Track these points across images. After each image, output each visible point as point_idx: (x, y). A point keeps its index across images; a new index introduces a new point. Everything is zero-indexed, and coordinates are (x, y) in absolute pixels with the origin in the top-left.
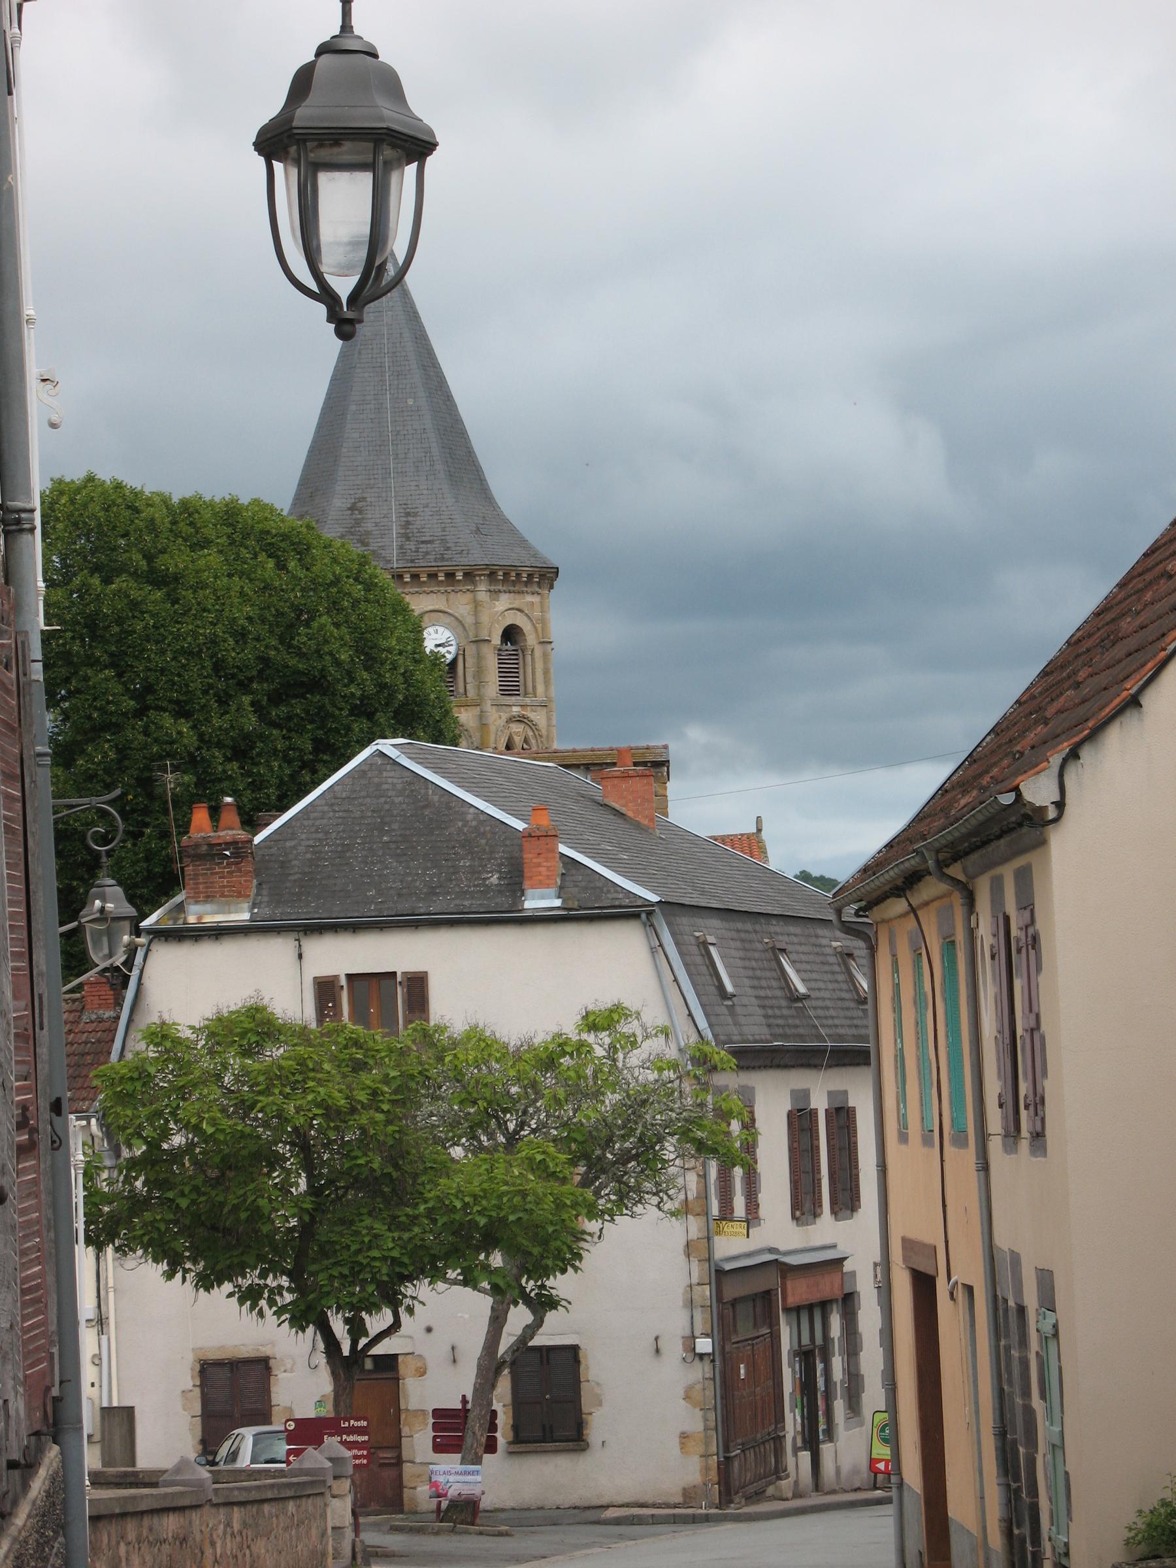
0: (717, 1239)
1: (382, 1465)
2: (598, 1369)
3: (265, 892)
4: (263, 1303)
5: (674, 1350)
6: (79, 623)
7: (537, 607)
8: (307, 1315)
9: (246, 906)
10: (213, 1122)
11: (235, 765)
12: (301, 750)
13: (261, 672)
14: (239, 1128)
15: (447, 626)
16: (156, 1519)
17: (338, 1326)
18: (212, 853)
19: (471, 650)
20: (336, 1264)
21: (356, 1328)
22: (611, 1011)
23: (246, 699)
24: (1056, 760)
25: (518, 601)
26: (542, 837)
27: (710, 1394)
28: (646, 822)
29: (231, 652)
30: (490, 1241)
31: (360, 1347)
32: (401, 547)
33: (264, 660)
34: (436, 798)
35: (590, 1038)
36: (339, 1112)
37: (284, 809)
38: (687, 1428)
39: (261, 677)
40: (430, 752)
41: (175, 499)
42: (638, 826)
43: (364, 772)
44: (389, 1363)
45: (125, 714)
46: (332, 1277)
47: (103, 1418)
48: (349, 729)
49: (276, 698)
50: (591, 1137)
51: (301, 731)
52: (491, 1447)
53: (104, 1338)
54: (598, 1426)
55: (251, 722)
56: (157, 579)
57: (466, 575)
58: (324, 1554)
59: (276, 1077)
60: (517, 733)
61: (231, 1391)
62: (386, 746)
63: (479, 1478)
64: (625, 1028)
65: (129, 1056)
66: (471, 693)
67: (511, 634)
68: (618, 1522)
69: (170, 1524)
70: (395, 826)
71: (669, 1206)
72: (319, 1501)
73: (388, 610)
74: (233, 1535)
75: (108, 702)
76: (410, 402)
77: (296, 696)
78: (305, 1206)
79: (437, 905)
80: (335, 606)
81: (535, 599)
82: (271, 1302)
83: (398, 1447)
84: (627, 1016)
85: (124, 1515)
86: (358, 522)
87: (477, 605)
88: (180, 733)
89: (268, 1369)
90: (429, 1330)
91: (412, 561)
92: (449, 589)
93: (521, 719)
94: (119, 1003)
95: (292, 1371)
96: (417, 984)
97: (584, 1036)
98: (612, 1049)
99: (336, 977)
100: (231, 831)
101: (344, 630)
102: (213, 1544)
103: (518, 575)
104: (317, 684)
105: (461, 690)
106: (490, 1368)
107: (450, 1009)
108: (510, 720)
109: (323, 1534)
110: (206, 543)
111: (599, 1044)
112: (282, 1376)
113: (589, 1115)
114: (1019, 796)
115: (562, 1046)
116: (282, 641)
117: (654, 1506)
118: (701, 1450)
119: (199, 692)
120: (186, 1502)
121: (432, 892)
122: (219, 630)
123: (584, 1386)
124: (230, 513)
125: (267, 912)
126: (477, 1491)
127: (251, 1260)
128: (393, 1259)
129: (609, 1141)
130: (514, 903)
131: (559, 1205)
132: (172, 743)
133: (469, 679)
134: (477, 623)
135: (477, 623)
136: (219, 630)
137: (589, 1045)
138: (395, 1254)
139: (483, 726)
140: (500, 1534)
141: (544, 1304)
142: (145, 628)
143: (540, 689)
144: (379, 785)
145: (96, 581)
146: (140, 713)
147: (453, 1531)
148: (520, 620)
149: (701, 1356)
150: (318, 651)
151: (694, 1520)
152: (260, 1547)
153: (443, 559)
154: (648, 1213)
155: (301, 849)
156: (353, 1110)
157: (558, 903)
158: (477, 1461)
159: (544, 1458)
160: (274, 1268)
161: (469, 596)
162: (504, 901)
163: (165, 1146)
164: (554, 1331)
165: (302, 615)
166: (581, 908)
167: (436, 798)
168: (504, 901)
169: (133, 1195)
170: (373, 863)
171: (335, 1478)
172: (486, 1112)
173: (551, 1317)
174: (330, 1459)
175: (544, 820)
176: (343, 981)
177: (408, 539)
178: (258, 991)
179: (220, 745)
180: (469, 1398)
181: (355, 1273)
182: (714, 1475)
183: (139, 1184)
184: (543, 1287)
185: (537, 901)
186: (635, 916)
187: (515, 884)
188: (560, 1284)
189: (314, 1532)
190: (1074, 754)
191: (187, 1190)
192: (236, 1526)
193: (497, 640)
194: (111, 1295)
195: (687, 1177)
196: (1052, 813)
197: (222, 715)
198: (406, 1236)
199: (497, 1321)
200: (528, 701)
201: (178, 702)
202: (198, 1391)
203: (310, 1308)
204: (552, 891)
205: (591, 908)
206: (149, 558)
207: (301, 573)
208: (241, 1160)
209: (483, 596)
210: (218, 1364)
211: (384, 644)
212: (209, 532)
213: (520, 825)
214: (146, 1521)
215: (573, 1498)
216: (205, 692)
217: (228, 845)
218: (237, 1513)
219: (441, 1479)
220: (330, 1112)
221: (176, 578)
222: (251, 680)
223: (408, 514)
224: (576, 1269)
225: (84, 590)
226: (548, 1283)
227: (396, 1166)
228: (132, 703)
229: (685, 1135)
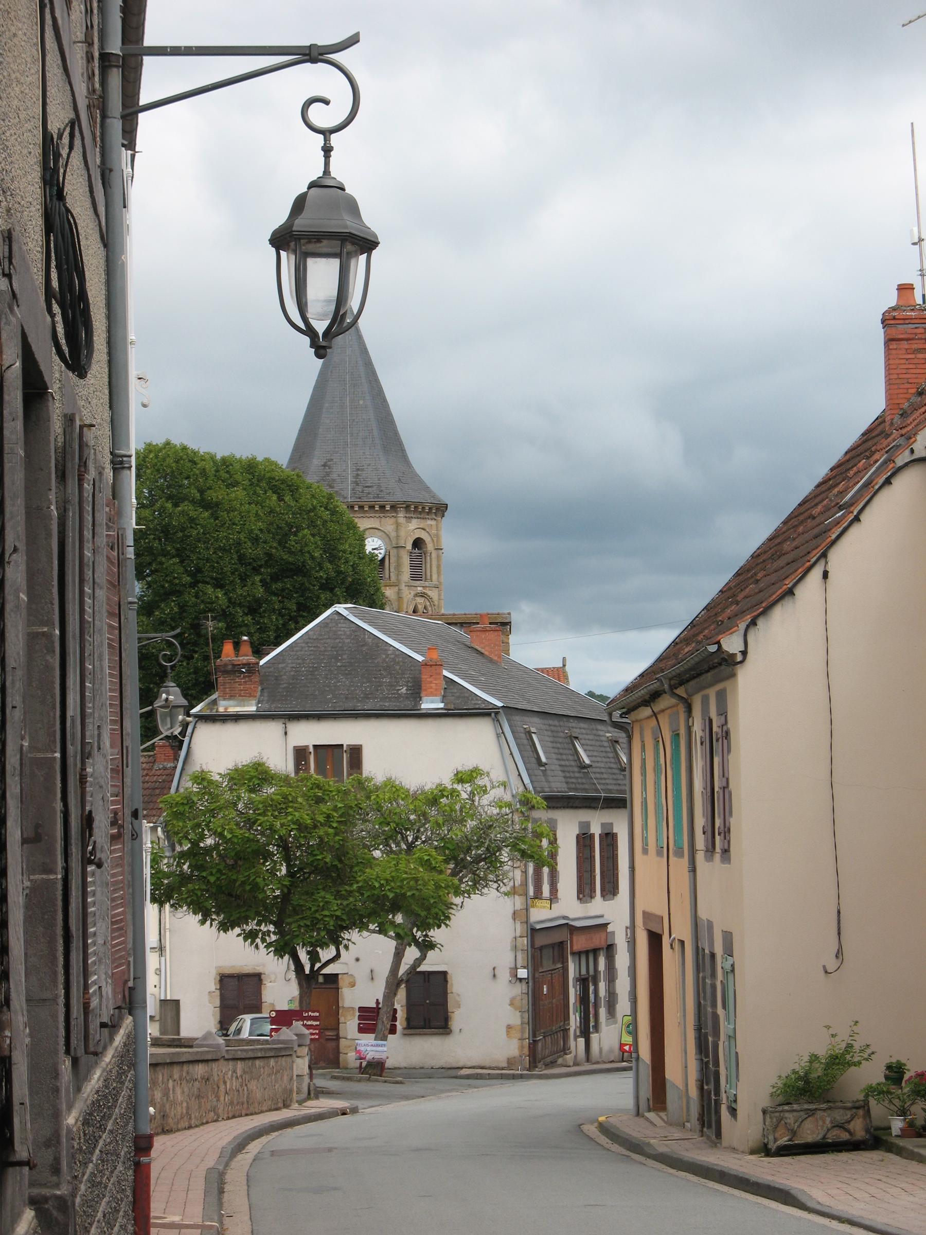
0: (532, 910)
1: (327, 1040)
2: (458, 986)
3: (266, 694)
4: (258, 940)
5: (504, 975)
6: (157, 530)
7: (434, 528)
8: (283, 948)
9: (254, 702)
10: (231, 831)
11: (250, 618)
13: (266, 562)
16: (191, 1067)
18: (234, 670)
19: (393, 552)
20: (302, 918)
21: (314, 957)
22: (472, 771)
23: (257, 578)
24: (742, 626)
26: (433, 666)
27: (525, 1003)
28: (496, 658)
29: (249, 550)
30: (395, 907)
31: (316, 968)
32: (353, 489)
33: (269, 555)
34: (370, 640)
35: (459, 787)
36: (306, 827)
37: (278, 644)
38: (511, 1022)
39: (267, 564)
40: (368, 613)
41: (218, 457)
42: (491, 661)
43: (327, 624)
44: (333, 979)
45: (184, 585)
46: (300, 926)
47: (161, 1006)
48: (318, 597)
49: (275, 578)
51: (290, 598)
52: (393, 1030)
53: (163, 959)
54: (458, 1019)
56: (206, 505)
57: (392, 507)
58: (291, 1091)
59: (270, 806)
60: (420, 603)
61: (238, 992)
62: (341, 608)
63: (385, 1049)
64: (480, 782)
65: (182, 790)
66: (393, 578)
67: (418, 543)
68: (468, 1077)
69: (200, 1070)
70: (345, 657)
71: (503, 889)
72: (288, 1059)
73: (345, 528)
74: (237, 1077)
75: (175, 578)
76: (361, 402)
80: (312, 524)
81: (433, 523)
82: (263, 940)
83: (338, 1029)
84: (481, 775)
85: (172, 1064)
86: (328, 474)
87: (398, 525)
88: (217, 597)
89: (260, 980)
90: (357, 960)
93: (423, 595)
94: (176, 759)
95: (275, 982)
96: (356, 752)
97: (455, 786)
98: (472, 794)
99: (307, 746)
100: (246, 657)
101: (318, 538)
102: (225, 1083)
103: (423, 508)
104: (299, 570)
105: (387, 576)
106: (393, 983)
107: (375, 768)
109: (291, 1079)
110: (235, 484)
111: (464, 791)
112: (269, 984)
114: (720, 647)
116: (280, 543)
117: (490, 1068)
119: (229, 573)
120: (209, 1057)
121: (367, 697)
122: (242, 536)
123: (449, 996)
124: (251, 466)
125: (267, 706)
126: (384, 1056)
127: (252, 915)
128: (337, 917)
129: (469, 849)
130: (415, 705)
131: (438, 887)
134: (398, 536)
135: (398, 536)
136: (242, 536)
137: (458, 792)
138: (338, 913)
139: (400, 598)
140: (397, 1082)
141: (427, 946)
142: (198, 534)
143: (435, 577)
145: (169, 505)
146: (193, 585)
147: (369, 1080)
148: (423, 535)
149: (521, 980)
150: (301, 551)
151: (514, 1077)
152: (253, 1085)
153: (378, 497)
155: (288, 669)
156: (315, 827)
157: (442, 705)
158: (384, 1038)
159: (425, 1038)
160: (265, 920)
161: (393, 520)
162: (409, 704)
163: (202, 845)
165: (292, 529)
167: (370, 640)
170: (331, 679)
171: (299, 1046)
172: (394, 830)
173: (431, 954)
175: (435, 655)
176: (311, 749)
179: (240, 605)
180: (381, 1001)
181: (314, 924)
182: (526, 1051)
183: (185, 867)
184: (426, 936)
185: (430, 704)
186: (489, 715)
187: (416, 693)
188: (436, 934)
189: (285, 1077)
190: (753, 623)
191: (214, 871)
192: (239, 1073)
194: (168, 933)
195: (515, 872)
196: (739, 658)
198: (345, 903)
199: (399, 955)
200: (427, 584)
201: (216, 579)
202: (218, 993)
203: (286, 944)
204: (438, 698)
205: (462, 709)
206: (202, 492)
207: (293, 504)
208: (246, 855)
209: (402, 520)
210: (231, 976)
212: (238, 477)
213: (420, 658)
214: (185, 1067)
215: (442, 1062)
216: (233, 573)
217: (244, 665)
218: (240, 1065)
219: (362, 1049)
221: (217, 505)
222: (261, 566)
223: (358, 470)
224: (447, 925)
225: (162, 510)
226: (430, 934)
227: (341, 861)
228: (188, 578)
229: (514, 846)
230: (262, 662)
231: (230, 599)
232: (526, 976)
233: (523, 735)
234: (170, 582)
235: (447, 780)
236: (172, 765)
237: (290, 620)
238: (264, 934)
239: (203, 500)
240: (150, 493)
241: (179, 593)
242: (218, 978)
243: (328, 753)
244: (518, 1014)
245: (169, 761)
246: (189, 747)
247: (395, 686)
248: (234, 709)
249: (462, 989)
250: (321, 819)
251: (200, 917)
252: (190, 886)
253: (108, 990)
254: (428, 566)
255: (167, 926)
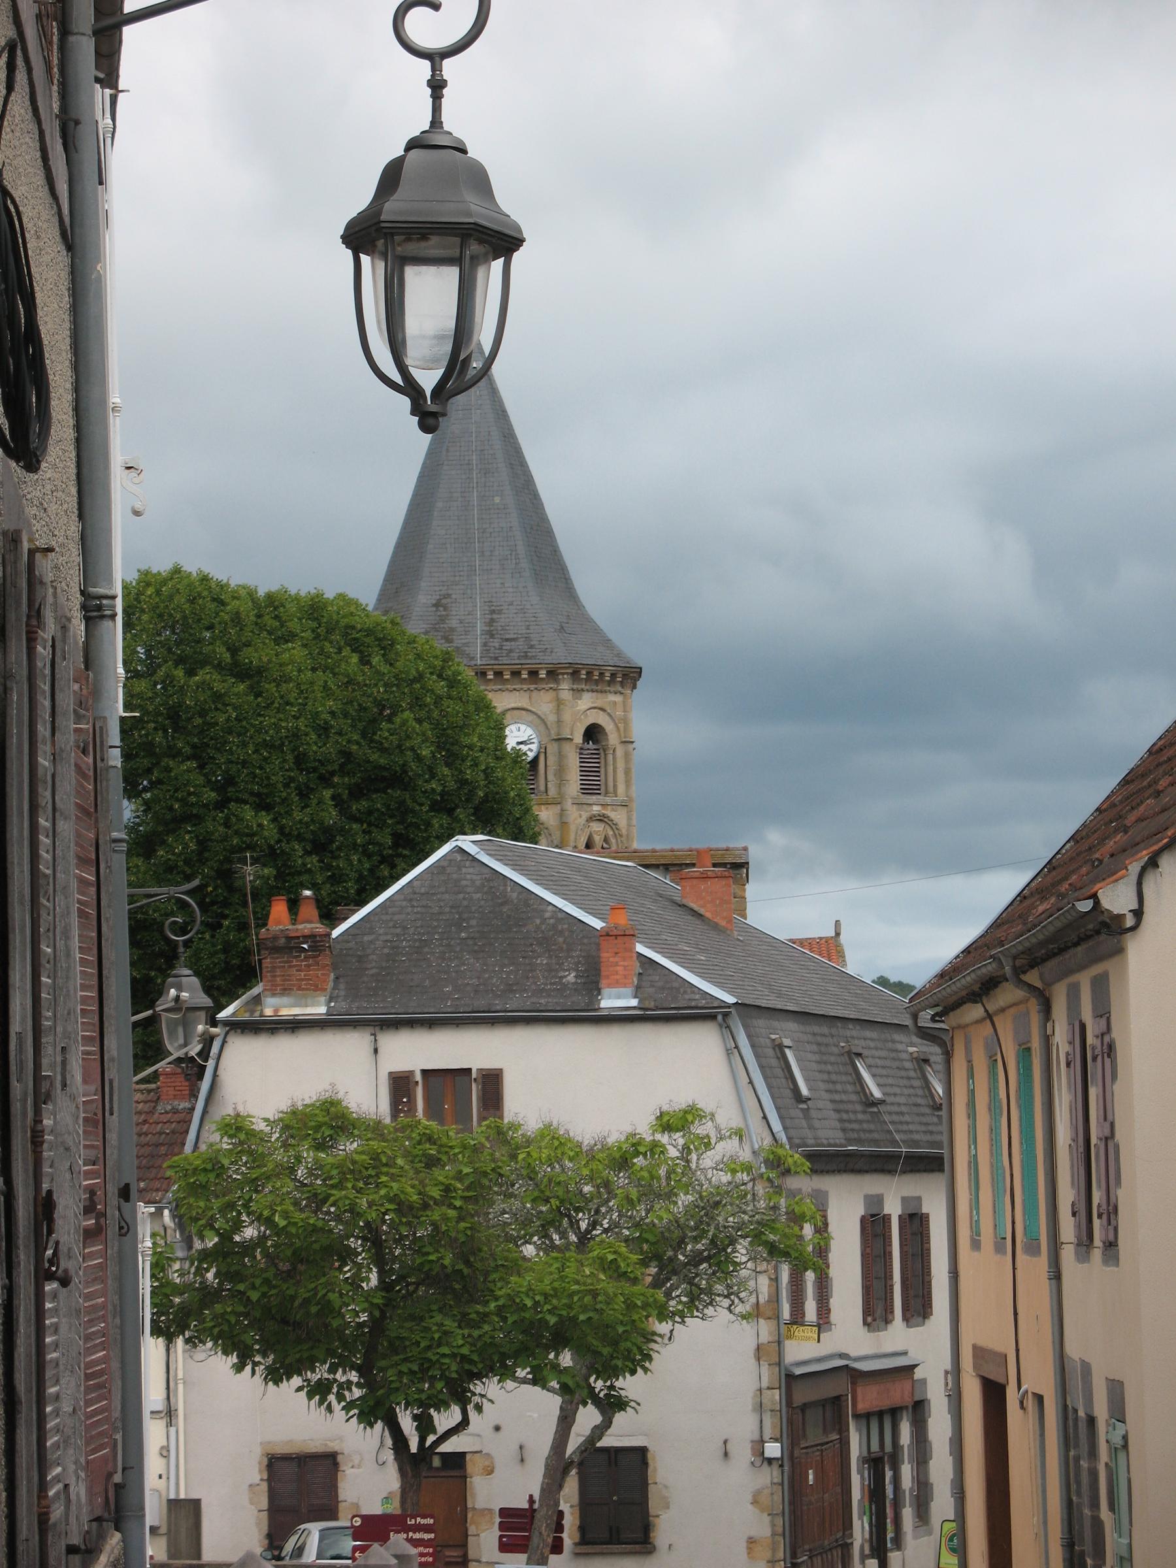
3: (342, 986)
4: (332, 1398)
5: (743, 1454)
8: (375, 1410)
9: (323, 999)
10: (286, 1215)
11: (315, 858)
12: (381, 845)
14: (311, 1221)
15: (529, 724)
17: (407, 1424)
18: (290, 946)
19: (552, 748)
20: (406, 1360)
21: (425, 1425)
22: (686, 1112)
23: (327, 794)
24: (1134, 868)
25: (601, 700)
26: (620, 936)
27: (778, 1500)
28: (723, 923)
29: (312, 745)
30: (560, 1340)
32: (485, 644)
33: (347, 755)
34: (515, 895)
35: (664, 1139)
37: (362, 903)
39: (342, 770)
41: (261, 592)
42: (716, 927)
44: (457, 1461)
45: (206, 806)
47: (169, 1510)
48: (428, 824)
49: (357, 792)
50: (663, 1238)
52: (557, 1548)
53: (172, 1430)
54: (665, 1529)
55: (331, 816)
56: (241, 672)
59: (350, 1171)
60: (597, 832)
62: (466, 842)
64: (700, 1129)
65: (203, 1147)
66: (552, 791)
67: (593, 733)
70: (473, 922)
71: (740, 1308)
73: (471, 708)
75: (190, 794)
76: (497, 500)
77: (377, 791)
78: (376, 1301)
79: (513, 1003)
80: (417, 702)
82: (340, 1397)
83: (464, 1545)
86: (442, 619)
87: (559, 703)
88: (260, 825)
89: (336, 1465)
90: (497, 1428)
91: (496, 658)
92: (532, 687)
93: (602, 819)
94: (194, 1095)
95: (359, 1466)
96: (492, 1081)
97: (658, 1136)
98: (686, 1149)
99: (412, 1072)
100: (309, 924)
103: (601, 674)
104: (397, 779)
105: (542, 788)
106: (557, 1468)
107: (524, 1107)
108: (591, 819)
110: (290, 637)
111: (673, 1144)
112: (349, 1472)
113: (660, 1216)
114: (1097, 903)
115: (635, 1146)
116: (364, 735)
118: (769, 1555)
119: (280, 786)
121: (510, 989)
122: (301, 723)
123: (651, 1488)
124: (315, 608)
125: (343, 1005)
128: (463, 1357)
129: (682, 1242)
131: (630, 1306)
132: (253, 835)
133: (550, 777)
134: (559, 722)
135: (559, 722)
136: (301, 723)
137: (663, 1146)
138: (465, 1351)
139: (563, 824)
141: (612, 1405)
142: (228, 720)
143: (621, 789)
144: (459, 880)
145: (179, 673)
146: (221, 805)
148: (602, 719)
149: (770, 1461)
153: (526, 657)
154: (719, 1315)
156: (425, 1206)
157: (634, 1002)
160: (344, 1363)
161: (551, 694)
162: (580, 1000)
163: (237, 1238)
164: (623, 1433)
165: (384, 710)
166: (657, 1009)
168: (580, 1000)
169: (204, 1286)
172: (558, 1211)
173: (619, 1418)
174: (396, 1556)
175: (622, 919)
176: (418, 1077)
177: (492, 636)
178: (333, 1085)
179: (300, 838)
180: (536, 1497)
181: (424, 1370)
183: (210, 1276)
184: (612, 1387)
185: (613, 1000)
186: (712, 1017)
187: (592, 984)
188: (630, 1385)
190: (1153, 863)
191: (258, 1282)
193: (579, 739)
194: (181, 1387)
195: (759, 1280)
196: (1129, 922)
197: (303, 808)
198: (476, 1333)
200: (608, 800)
201: (259, 795)
202: (265, 1486)
203: (379, 1403)
204: (629, 991)
205: (667, 1008)
206: (234, 651)
207: (384, 668)
208: (311, 1254)
209: (566, 695)
210: (286, 1458)
211: (466, 741)
213: (597, 924)
217: (306, 938)
220: (402, 1207)
222: (333, 774)
223: (493, 612)
224: (646, 1370)
226: (618, 1384)
227: (467, 1263)
228: (213, 794)
229: (757, 1237)
230: (335, 933)
231: (281, 830)
232: (778, 1454)
233: (770, 1052)
234: (184, 802)
235: (644, 1127)
236: (184, 1105)
237: (381, 863)
238: (341, 1386)
239: (236, 664)
240: (148, 652)
241: (197, 819)
242: (265, 1461)
243: (446, 1082)
244: (766, 1519)
245: (183, 1098)
246: (215, 1075)
247: (557, 971)
248: (290, 1010)
249: (670, 1474)
250: (435, 1193)
251: (233, 1359)
252: (218, 1308)
253: (79, 1491)
254: (610, 769)
255: (180, 1375)
